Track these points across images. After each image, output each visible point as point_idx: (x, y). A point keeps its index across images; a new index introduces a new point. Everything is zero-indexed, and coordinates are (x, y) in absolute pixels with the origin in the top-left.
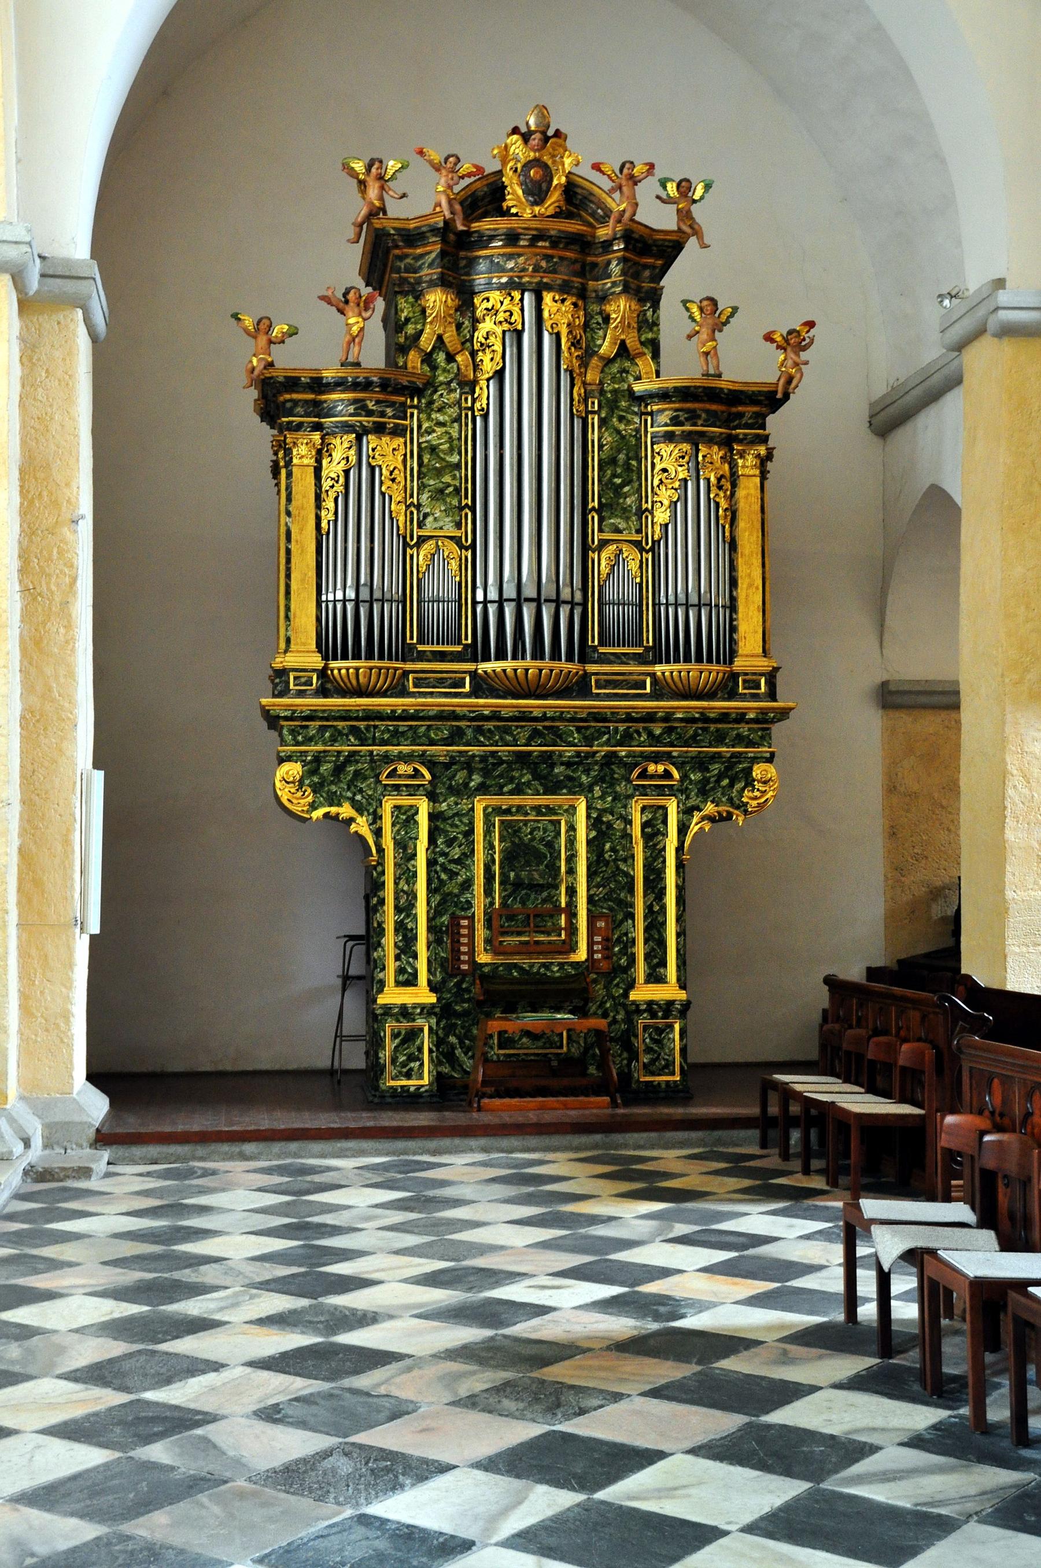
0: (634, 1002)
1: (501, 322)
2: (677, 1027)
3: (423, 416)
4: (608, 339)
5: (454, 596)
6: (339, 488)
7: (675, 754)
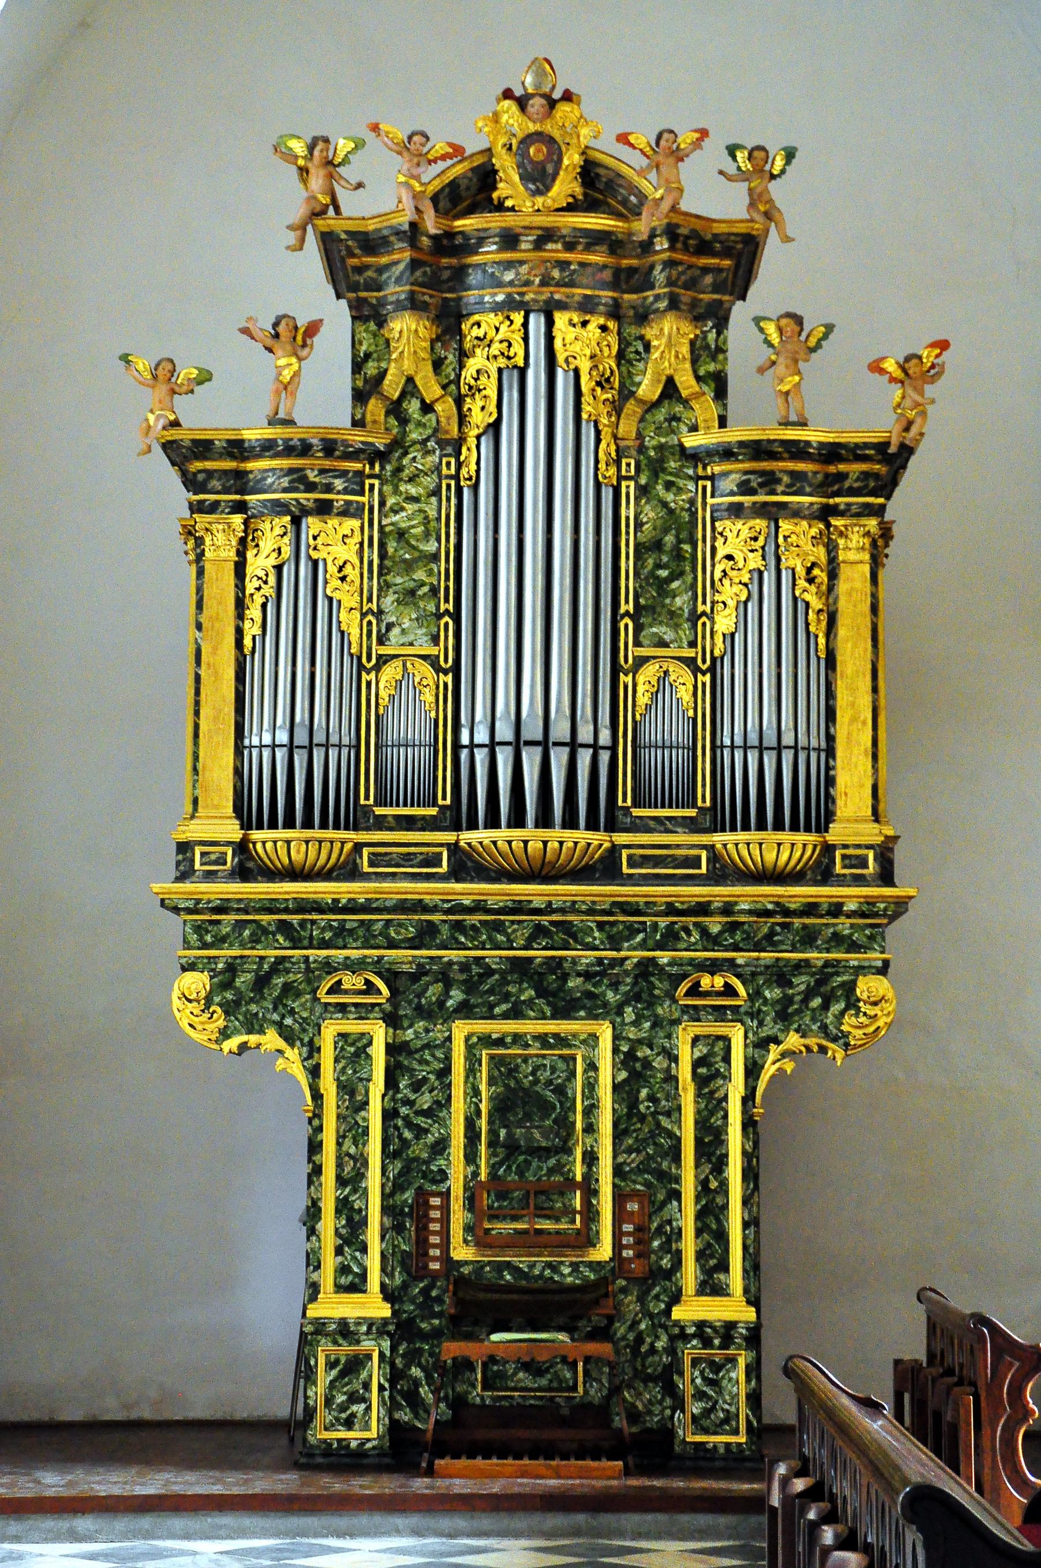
0: (677, 1323)
1: (495, 357)
2: (742, 1362)
3: (388, 489)
4: (648, 376)
5: (427, 738)
6: (269, 590)
7: (740, 961)
